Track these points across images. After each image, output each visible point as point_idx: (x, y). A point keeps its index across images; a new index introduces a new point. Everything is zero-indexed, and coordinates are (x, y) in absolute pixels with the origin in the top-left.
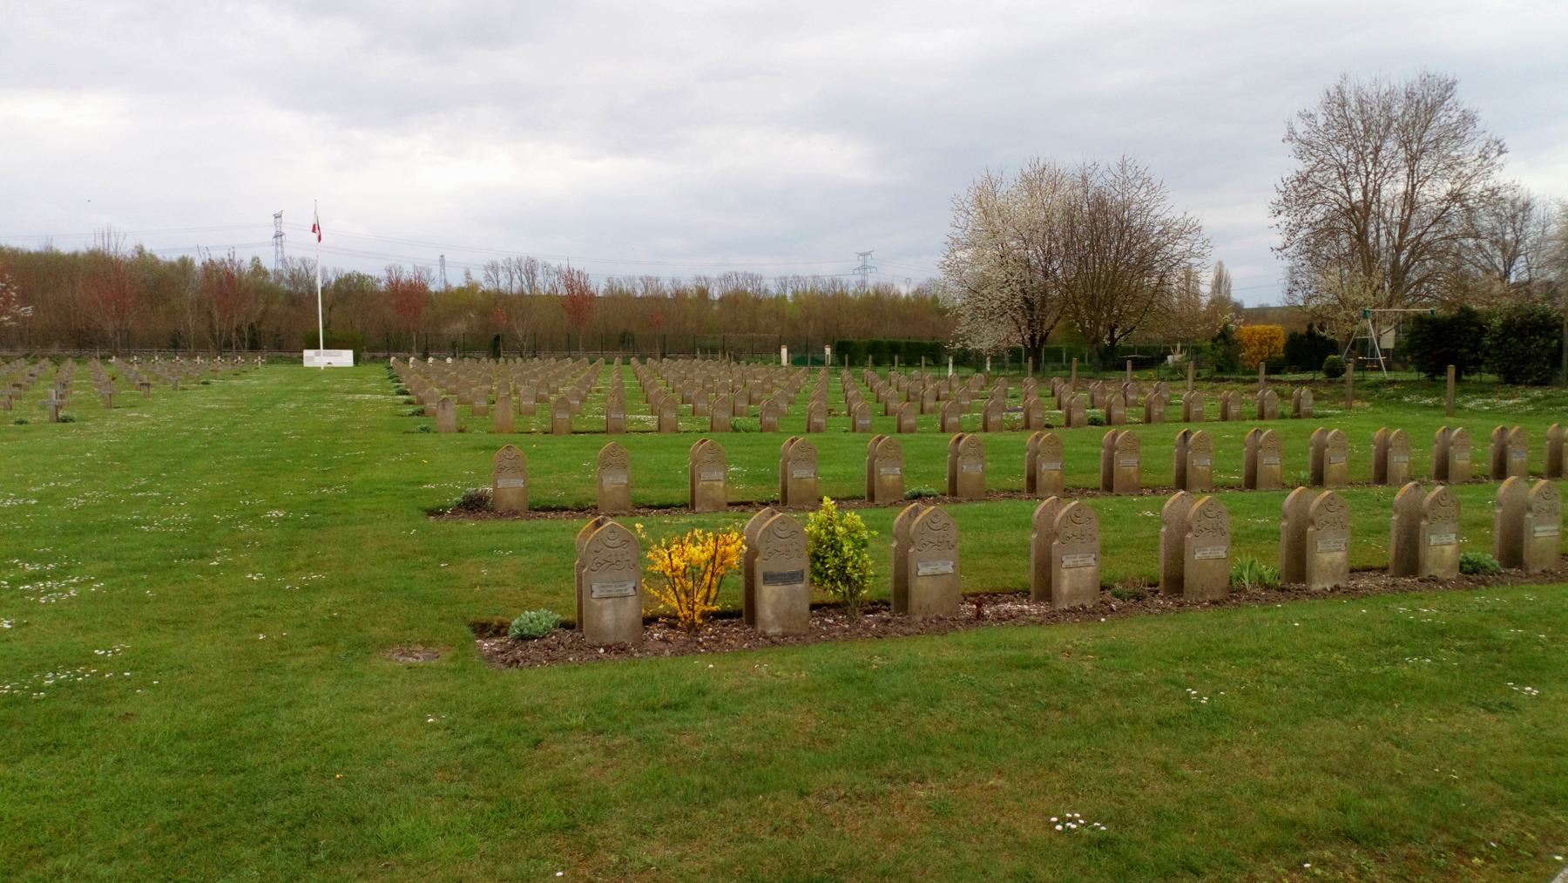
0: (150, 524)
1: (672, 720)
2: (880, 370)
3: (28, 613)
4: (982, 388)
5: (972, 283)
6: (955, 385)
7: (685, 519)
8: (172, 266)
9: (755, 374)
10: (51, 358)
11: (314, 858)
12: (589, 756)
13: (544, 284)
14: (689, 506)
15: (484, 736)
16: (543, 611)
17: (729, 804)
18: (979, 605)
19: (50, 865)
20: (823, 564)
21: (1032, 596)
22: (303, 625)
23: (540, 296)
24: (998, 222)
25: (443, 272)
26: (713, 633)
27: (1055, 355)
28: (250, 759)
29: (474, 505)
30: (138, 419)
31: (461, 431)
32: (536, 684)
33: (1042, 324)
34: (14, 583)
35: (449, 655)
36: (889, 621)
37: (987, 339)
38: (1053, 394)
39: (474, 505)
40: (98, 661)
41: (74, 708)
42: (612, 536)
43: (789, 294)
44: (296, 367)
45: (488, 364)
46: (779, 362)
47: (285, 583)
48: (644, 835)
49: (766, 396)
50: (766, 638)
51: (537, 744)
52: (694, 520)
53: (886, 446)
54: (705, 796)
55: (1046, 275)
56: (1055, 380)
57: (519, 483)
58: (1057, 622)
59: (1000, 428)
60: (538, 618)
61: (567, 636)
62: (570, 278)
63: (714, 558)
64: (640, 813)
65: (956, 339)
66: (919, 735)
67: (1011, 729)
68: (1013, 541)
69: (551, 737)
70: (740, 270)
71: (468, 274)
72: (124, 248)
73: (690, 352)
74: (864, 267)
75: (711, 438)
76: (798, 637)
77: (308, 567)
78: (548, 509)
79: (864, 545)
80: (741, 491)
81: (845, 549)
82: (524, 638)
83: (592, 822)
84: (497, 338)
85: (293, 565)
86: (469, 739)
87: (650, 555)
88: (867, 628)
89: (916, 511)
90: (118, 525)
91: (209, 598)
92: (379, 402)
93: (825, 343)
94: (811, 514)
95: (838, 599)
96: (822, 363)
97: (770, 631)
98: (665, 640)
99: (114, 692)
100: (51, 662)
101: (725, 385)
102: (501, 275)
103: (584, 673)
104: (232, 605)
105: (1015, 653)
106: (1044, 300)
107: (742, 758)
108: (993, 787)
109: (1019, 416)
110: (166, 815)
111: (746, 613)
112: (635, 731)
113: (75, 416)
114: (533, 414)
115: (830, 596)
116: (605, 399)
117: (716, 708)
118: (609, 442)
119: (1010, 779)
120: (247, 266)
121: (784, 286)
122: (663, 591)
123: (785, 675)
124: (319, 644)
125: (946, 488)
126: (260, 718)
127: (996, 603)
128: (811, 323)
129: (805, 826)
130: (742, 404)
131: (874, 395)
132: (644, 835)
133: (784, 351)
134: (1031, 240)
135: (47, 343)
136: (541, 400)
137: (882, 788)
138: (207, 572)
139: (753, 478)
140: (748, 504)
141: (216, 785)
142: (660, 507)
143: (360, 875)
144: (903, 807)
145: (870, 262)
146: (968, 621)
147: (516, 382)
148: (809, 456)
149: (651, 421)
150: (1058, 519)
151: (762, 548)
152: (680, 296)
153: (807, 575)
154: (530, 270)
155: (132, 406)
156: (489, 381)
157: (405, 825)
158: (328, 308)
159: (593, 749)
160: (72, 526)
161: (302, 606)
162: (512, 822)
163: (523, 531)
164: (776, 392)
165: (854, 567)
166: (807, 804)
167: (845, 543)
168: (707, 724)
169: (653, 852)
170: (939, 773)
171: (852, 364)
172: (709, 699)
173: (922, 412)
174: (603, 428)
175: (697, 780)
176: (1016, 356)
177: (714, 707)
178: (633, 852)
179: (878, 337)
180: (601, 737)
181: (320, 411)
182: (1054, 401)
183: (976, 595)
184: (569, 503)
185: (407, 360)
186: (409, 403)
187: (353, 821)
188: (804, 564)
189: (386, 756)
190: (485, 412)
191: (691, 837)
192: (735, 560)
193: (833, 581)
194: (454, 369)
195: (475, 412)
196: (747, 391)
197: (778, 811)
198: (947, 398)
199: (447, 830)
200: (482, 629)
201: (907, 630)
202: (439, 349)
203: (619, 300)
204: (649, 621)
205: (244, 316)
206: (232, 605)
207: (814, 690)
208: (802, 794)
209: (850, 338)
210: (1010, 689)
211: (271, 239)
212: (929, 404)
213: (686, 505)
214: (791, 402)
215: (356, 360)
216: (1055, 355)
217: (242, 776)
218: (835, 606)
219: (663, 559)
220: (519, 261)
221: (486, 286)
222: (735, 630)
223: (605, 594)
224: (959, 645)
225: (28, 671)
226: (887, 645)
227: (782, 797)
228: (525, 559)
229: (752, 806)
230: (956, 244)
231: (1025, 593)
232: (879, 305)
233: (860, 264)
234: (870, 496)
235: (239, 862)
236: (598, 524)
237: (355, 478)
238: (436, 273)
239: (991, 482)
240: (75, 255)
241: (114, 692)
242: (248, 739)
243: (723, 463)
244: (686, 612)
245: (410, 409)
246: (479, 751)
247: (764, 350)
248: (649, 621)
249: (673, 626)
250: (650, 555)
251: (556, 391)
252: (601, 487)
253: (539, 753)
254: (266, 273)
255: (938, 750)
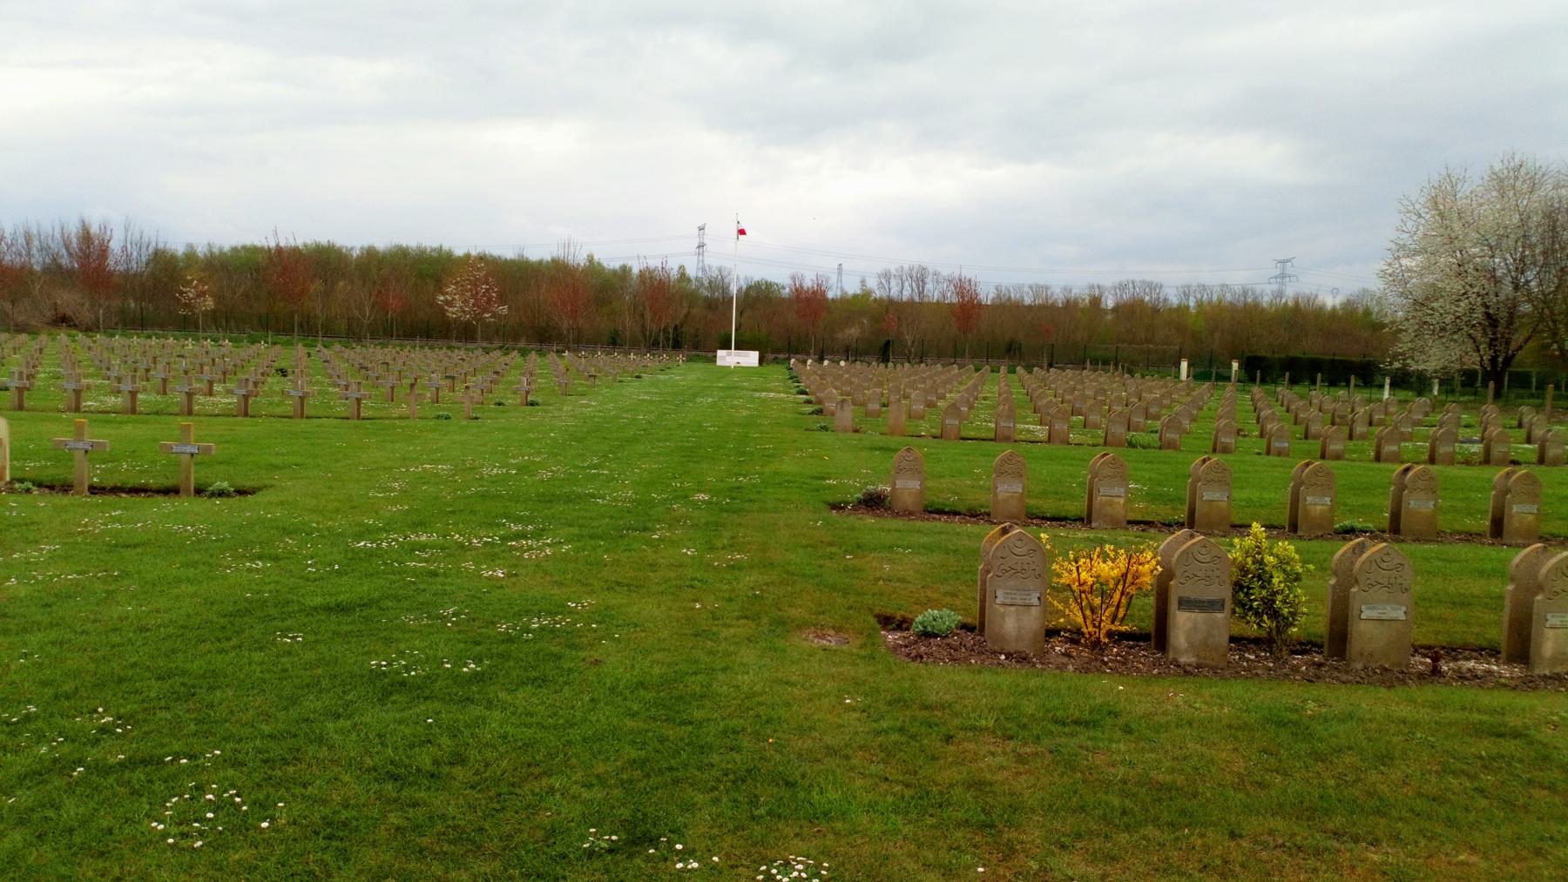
0: (603, 498)
1: (1083, 737)
2: (1297, 388)
3: (516, 566)
4: (1426, 414)
5: (1419, 294)
6: (1392, 409)
7: (1082, 534)
8: (614, 272)
9: (1152, 388)
10: (520, 350)
11: (757, 813)
12: (1000, 759)
13: (933, 292)
14: (1085, 520)
15: (899, 724)
16: (946, 611)
17: (1150, 831)
18: (1436, 659)
19: (544, 781)
20: (1247, 594)
21: (1503, 655)
22: (731, 600)
23: (929, 303)
24: (1457, 226)
25: (840, 280)
26: (1118, 654)
27: (1522, 381)
28: (698, 714)
29: (873, 502)
30: (588, 406)
31: (856, 431)
32: (941, 680)
33: (1508, 343)
34: (504, 539)
35: (859, 642)
36: (1320, 665)
37: (1434, 358)
38: (1520, 425)
39: (873, 502)
40: (571, 612)
41: (556, 649)
42: (1019, 543)
43: (1192, 304)
44: (709, 366)
45: (877, 369)
46: (1177, 376)
47: (713, 560)
48: (1063, 847)
49: (1164, 411)
50: (1178, 666)
51: (948, 739)
52: (1092, 536)
53: (1315, 473)
54: (1126, 819)
55: (1516, 288)
56: (1524, 409)
57: (915, 485)
58: (1535, 688)
59: (1451, 460)
60: (944, 617)
61: (969, 639)
62: (962, 287)
63: (1124, 576)
64: (1057, 824)
65: (1395, 357)
66: (1370, 794)
67: (1484, 803)
68: (1476, 592)
69: (961, 734)
70: (1138, 278)
71: (863, 282)
72: (579, 258)
73: (1079, 362)
74: (1283, 276)
75: (1112, 452)
76: (1214, 669)
77: (732, 546)
78: (941, 512)
79: (1298, 578)
80: (1141, 509)
81: (1275, 580)
82: (927, 635)
83: (1010, 824)
84: (888, 343)
85: (719, 544)
86: (885, 725)
87: (1055, 566)
88: (1295, 669)
89: (1361, 548)
90: (579, 496)
91: (653, 566)
92: (782, 400)
93: (1233, 357)
94: (1236, 540)
95: (1264, 634)
96: (1228, 379)
97: (1183, 660)
98: (1067, 655)
99: (585, 640)
100: (536, 608)
101: (1119, 398)
102: (893, 283)
103: (987, 677)
104: (673, 575)
105: (1484, 718)
106: (1511, 315)
107: (1161, 787)
108: (1463, 863)
109: (1476, 448)
110: (634, 754)
111: (1158, 637)
112: (1046, 741)
113: (540, 400)
114: (922, 418)
115: (1253, 630)
116: (994, 407)
117: (1130, 732)
118: (1007, 449)
119: (1486, 857)
120: (674, 274)
121: (1187, 295)
122: (1065, 602)
123: (1204, 707)
124: (747, 618)
125: (1386, 524)
126: (700, 678)
127: (1455, 659)
128: (1217, 335)
129: (1238, 869)
130: (1138, 419)
131: (1291, 416)
132: (1063, 847)
133: (1184, 365)
134: (1498, 246)
135: (516, 339)
136: (931, 405)
137: (1329, 843)
138: (650, 543)
139: (1153, 497)
140: (1150, 524)
141: (671, 732)
142: (1053, 519)
143: (797, 835)
144: (1353, 868)
145: (1289, 270)
146: (1421, 676)
147: (907, 385)
148: (1223, 478)
149: (1041, 432)
150: (1544, 571)
151: (1178, 573)
152: (1070, 306)
153: (1229, 605)
154: (920, 278)
155: (582, 395)
156: (880, 384)
157: (832, 795)
158: (740, 313)
159: (1005, 753)
160: (543, 495)
161: (730, 583)
162: (931, 811)
163: (919, 532)
164: (1177, 408)
165: (1284, 602)
166: (1239, 845)
167: (1275, 574)
168: (1122, 747)
169: (1063, 864)
170: (1396, 838)
171: (1263, 381)
172: (1121, 721)
173: (1351, 437)
174: (992, 435)
175: (1116, 802)
176: (1469, 378)
177: (1127, 730)
178: (1052, 862)
179: (1296, 352)
180: (1012, 743)
181: (733, 407)
182: (1523, 433)
183: (1429, 648)
184: (962, 508)
185: (805, 362)
186: (809, 402)
187: (787, 784)
188: (1226, 593)
189: (811, 728)
190: (878, 414)
191: (1113, 859)
192: (1148, 580)
193: (1257, 614)
194: (847, 371)
195: (868, 414)
196: (1143, 404)
197: (1207, 848)
198: (1381, 423)
199: (871, 807)
200: (886, 621)
201: (1344, 678)
202: (833, 353)
203: (1008, 308)
204: (1051, 633)
205: (667, 319)
206: (673, 575)
207: (1239, 728)
208: (1233, 836)
209: (1262, 353)
210: (1481, 758)
211: (694, 249)
212: (1360, 429)
213: (1082, 520)
214: (1194, 419)
215: (761, 361)
216: (1522, 381)
217: (690, 728)
218: (1257, 641)
219: (1066, 572)
220: (911, 269)
221: (878, 293)
222: (1143, 656)
223: (1008, 601)
224: (1412, 701)
225: (519, 615)
226: (1319, 690)
227: (1209, 834)
228: (924, 559)
229: (1177, 839)
230: (1402, 250)
231: (1493, 652)
232: (1299, 317)
233: (1278, 272)
234: (1292, 528)
235: (694, 805)
236: (1005, 531)
237: (767, 469)
238: (833, 280)
239: (1444, 522)
240: (540, 262)
241: (585, 640)
242: (693, 695)
243: (1124, 479)
244: (1091, 629)
245: (810, 408)
246: (894, 737)
247: (1163, 363)
248: (1051, 633)
249: (1076, 642)
250: (1055, 566)
251: (942, 397)
252: (996, 495)
253: (952, 748)
254: (689, 280)
255: (1394, 813)
